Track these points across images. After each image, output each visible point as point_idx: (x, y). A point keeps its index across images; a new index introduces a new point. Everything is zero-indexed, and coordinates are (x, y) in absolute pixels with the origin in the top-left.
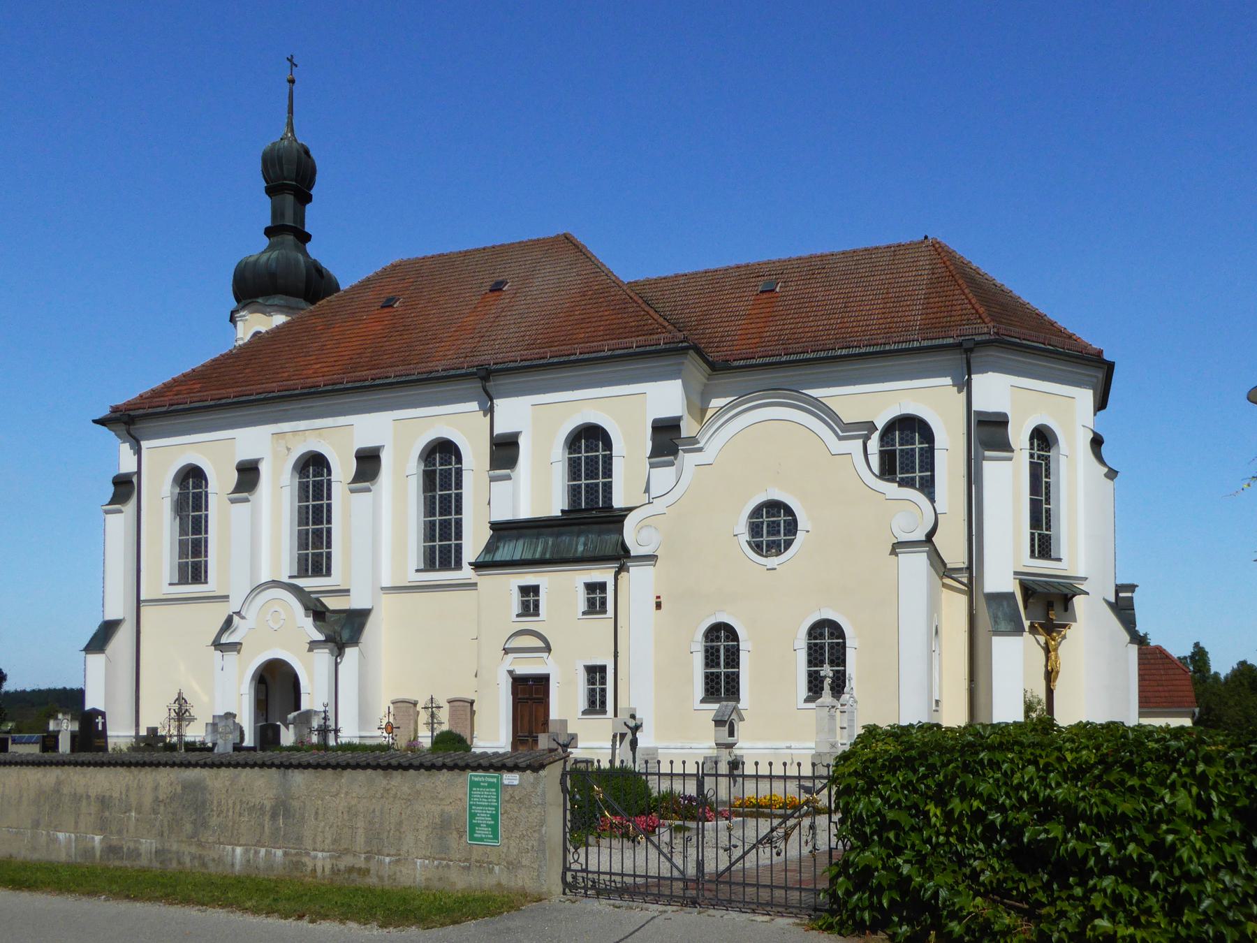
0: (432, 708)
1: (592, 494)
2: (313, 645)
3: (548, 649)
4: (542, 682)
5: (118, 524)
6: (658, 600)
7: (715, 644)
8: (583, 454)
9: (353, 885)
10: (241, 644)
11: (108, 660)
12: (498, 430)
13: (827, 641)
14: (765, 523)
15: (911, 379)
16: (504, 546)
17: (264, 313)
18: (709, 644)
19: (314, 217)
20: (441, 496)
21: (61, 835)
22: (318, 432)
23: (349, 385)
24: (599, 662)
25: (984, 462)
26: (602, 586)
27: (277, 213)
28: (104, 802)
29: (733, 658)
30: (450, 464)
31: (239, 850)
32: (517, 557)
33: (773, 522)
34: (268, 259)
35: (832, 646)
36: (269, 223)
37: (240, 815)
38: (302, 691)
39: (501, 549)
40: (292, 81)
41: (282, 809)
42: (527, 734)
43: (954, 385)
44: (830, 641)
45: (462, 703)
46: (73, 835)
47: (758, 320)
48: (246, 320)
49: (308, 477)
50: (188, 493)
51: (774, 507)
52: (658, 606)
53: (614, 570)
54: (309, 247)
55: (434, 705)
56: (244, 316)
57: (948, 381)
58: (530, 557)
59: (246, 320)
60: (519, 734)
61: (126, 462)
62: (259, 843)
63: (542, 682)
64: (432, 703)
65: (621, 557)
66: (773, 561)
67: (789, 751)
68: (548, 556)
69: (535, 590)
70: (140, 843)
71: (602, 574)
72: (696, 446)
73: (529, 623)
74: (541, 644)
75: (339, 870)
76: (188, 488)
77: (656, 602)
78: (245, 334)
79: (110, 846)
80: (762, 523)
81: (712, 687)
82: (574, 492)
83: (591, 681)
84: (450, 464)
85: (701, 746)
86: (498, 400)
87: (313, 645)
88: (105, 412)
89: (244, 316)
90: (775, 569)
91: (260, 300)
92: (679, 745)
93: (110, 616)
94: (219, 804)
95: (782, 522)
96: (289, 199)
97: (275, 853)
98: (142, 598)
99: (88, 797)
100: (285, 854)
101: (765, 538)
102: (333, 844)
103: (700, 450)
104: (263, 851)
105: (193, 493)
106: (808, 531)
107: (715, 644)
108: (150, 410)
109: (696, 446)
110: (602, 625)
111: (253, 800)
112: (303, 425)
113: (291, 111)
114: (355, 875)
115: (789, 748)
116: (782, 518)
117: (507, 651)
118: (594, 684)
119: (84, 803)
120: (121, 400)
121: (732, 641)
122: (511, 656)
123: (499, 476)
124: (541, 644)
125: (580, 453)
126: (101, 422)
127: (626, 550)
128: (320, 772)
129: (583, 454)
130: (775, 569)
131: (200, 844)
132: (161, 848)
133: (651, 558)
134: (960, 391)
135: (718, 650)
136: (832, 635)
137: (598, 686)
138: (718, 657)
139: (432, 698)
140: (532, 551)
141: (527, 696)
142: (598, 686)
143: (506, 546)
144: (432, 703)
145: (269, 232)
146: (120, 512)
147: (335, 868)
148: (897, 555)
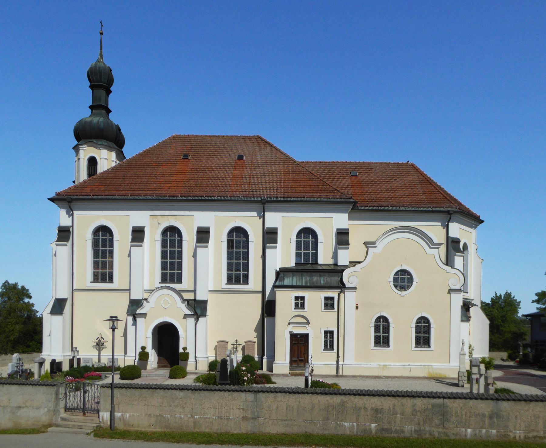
0: (236, 345)
1: (306, 257)
2: (186, 316)
3: (308, 323)
4: (306, 337)
5: (63, 251)
6: (357, 306)
7: (378, 324)
8: (303, 240)
9: (402, 435)
10: (147, 314)
11: (63, 317)
12: (267, 226)
13: (422, 324)
14: (399, 278)
15: (426, 222)
16: (287, 279)
17: (96, 148)
18: (376, 324)
19: (113, 101)
20: (236, 251)
21: (346, 424)
22: (175, 217)
23: (194, 198)
24: (330, 329)
25: (455, 257)
26: (332, 299)
27: (94, 99)
28: (377, 411)
29: (387, 329)
30: (241, 238)
31: (469, 430)
32: (294, 284)
33: (403, 278)
34: (98, 121)
35: (424, 327)
36: (90, 103)
37: (470, 417)
38: (180, 337)
39: (286, 280)
40: (101, 34)
41: (495, 415)
42: (297, 358)
43: (442, 226)
44: (423, 325)
45: (251, 343)
46: (355, 424)
47: (173, 148)
48: (85, 150)
49: (167, 237)
50: (99, 239)
51: (403, 272)
52: (357, 308)
53: (338, 292)
54: (110, 114)
55: (237, 343)
56: (84, 147)
57: (440, 224)
58: (300, 284)
59: (85, 150)
60: (293, 358)
61: (65, 220)
62: (482, 428)
63: (306, 337)
64: (236, 342)
65: (341, 287)
66: (403, 293)
67: (409, 366)
68: (308, 285)
69: (303, 298)
70: (404, 427)
71: (333, 294)
72: (374, 245)
73: (300, 312)
74: (305, 321)
75: (529, 437)
76: (99, 236)
77: (356, 307)
78: (85, 156)
79: (383, 428)
80: (398, 277)
81: (377, 341)
82: (298, 255)
83: (326, 337)
84: (241, 238)
85: (374, 364)
86: (267, 213)
87: (186, 316)
88: (53, 195)
89: (84, 147)
90: (404, 296)
91: (94, 141)
92: (365, 363)
93: (60, 296)
94: (456, 412)
95: (406, 278)
96: (103, 92)
97: (492, 431)
98: (74, 288)
99: (365, 408)
100: (498, 432)
101: (399, 284)
102: (525, 428)
103: (375, 247)
104: (484, 431)
105: (102, 239)
106: (417, 282)
107: (378, 324)
108: (81, 197)
109: (374, 245)
110: (332, 315)
111: (478, 412)
112: (167, 213)
113: (101, 49)
114: (538, 439)
115: (409, 365)
116: (406, 276)
117: (289, 323)
118: (326, 338)
119: (363, 411)
120: (61, 189)
121: (385, 323)
122: (291, 325)
123: (270, 247)
124: (305, 321)
125: (301, 239)
126: (52, 200)
127: (343, 285)
128: (518, 403)
129: (303, 240)
130: (404, 296)
131: (444, 427)
132: (418, 429)
133: (354, 289)
134: (444, 228)
135: (380, 326)
136: (424, 322)
137: (329, 339)
138: (380, 329)
139: (236, 341)
140: (301, 282)
141: (297, 342)
142: (329, 339)
143: (288, 279)
144: (236, 342)
145: (91, 107)
146: (66, 245)
147: (527, 437)
148: (450, 294)
